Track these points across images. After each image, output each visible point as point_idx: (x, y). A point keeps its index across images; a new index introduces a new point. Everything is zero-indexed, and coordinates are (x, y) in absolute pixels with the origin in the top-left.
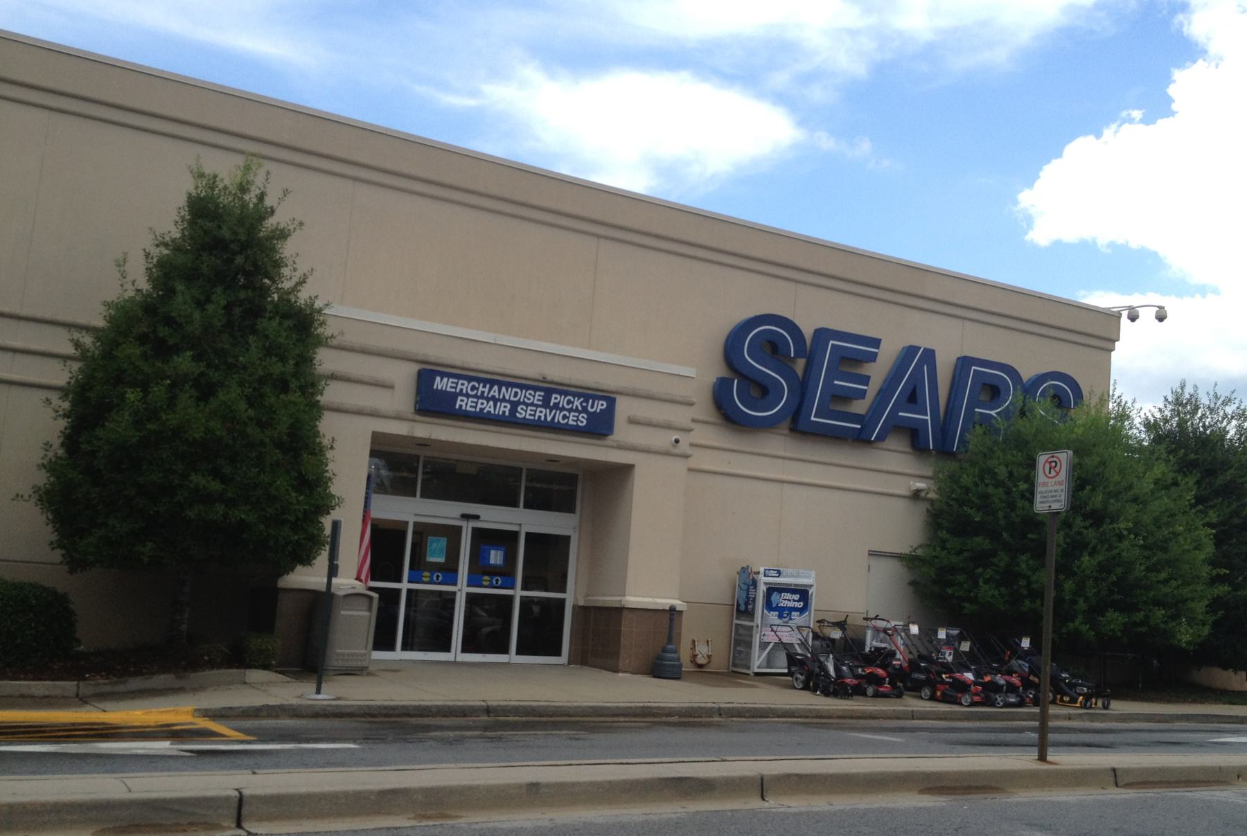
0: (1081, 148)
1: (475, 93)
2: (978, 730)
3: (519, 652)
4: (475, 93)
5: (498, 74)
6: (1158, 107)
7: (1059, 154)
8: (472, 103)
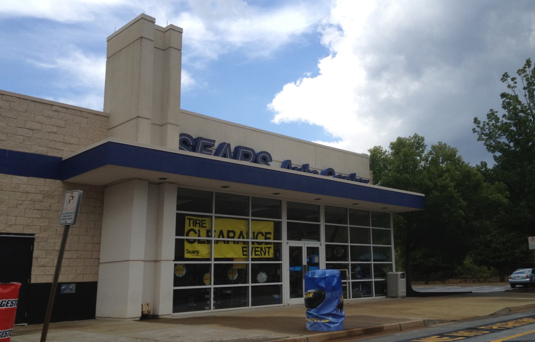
0: (289, 88)
1: (53, 62)
2: (523, 301)
3: (252, 306)
4: (53, 62)
5: (64, 55)
6: (316, 73)
7: (282, 90)
8: (52, 66)
